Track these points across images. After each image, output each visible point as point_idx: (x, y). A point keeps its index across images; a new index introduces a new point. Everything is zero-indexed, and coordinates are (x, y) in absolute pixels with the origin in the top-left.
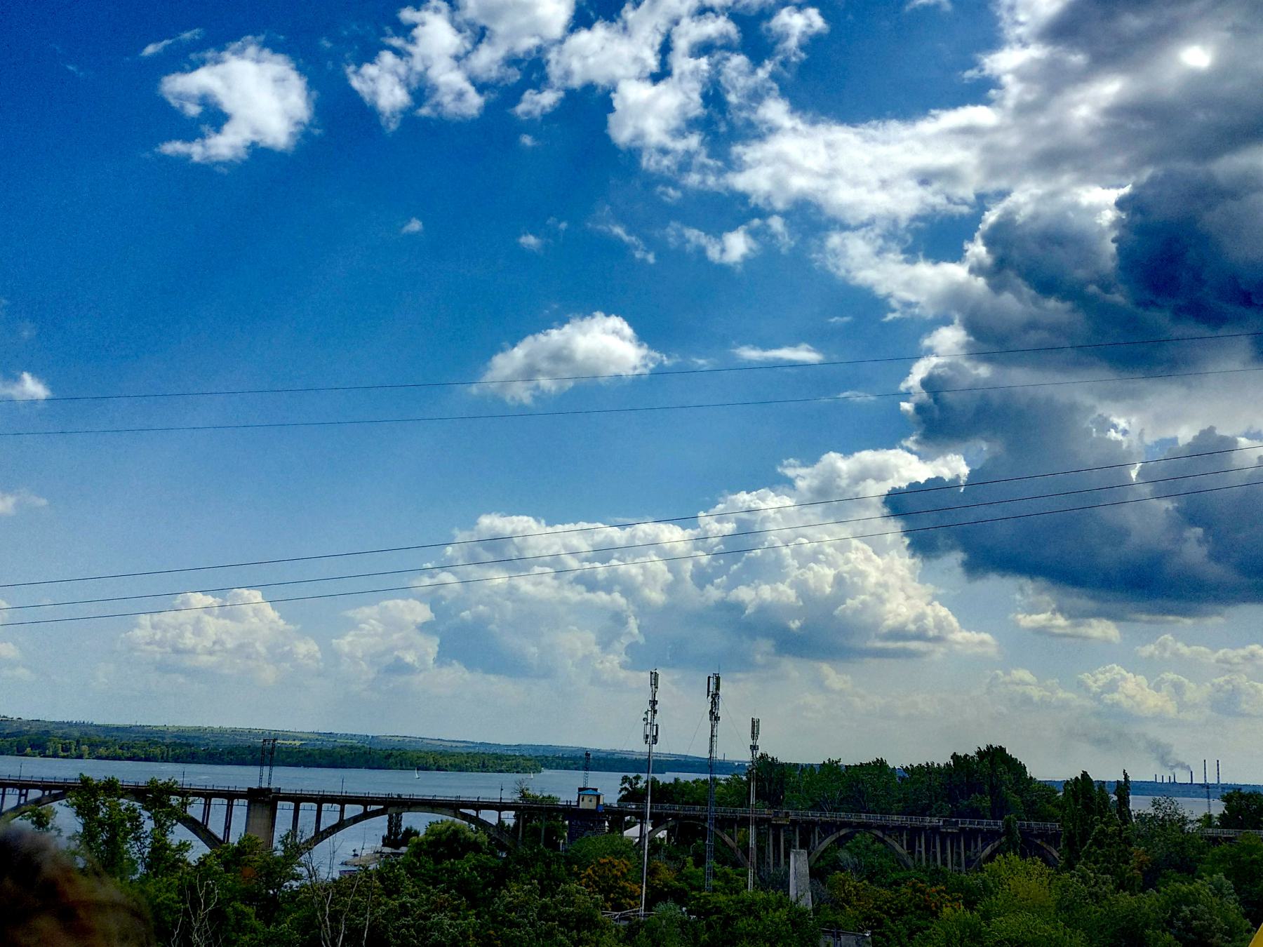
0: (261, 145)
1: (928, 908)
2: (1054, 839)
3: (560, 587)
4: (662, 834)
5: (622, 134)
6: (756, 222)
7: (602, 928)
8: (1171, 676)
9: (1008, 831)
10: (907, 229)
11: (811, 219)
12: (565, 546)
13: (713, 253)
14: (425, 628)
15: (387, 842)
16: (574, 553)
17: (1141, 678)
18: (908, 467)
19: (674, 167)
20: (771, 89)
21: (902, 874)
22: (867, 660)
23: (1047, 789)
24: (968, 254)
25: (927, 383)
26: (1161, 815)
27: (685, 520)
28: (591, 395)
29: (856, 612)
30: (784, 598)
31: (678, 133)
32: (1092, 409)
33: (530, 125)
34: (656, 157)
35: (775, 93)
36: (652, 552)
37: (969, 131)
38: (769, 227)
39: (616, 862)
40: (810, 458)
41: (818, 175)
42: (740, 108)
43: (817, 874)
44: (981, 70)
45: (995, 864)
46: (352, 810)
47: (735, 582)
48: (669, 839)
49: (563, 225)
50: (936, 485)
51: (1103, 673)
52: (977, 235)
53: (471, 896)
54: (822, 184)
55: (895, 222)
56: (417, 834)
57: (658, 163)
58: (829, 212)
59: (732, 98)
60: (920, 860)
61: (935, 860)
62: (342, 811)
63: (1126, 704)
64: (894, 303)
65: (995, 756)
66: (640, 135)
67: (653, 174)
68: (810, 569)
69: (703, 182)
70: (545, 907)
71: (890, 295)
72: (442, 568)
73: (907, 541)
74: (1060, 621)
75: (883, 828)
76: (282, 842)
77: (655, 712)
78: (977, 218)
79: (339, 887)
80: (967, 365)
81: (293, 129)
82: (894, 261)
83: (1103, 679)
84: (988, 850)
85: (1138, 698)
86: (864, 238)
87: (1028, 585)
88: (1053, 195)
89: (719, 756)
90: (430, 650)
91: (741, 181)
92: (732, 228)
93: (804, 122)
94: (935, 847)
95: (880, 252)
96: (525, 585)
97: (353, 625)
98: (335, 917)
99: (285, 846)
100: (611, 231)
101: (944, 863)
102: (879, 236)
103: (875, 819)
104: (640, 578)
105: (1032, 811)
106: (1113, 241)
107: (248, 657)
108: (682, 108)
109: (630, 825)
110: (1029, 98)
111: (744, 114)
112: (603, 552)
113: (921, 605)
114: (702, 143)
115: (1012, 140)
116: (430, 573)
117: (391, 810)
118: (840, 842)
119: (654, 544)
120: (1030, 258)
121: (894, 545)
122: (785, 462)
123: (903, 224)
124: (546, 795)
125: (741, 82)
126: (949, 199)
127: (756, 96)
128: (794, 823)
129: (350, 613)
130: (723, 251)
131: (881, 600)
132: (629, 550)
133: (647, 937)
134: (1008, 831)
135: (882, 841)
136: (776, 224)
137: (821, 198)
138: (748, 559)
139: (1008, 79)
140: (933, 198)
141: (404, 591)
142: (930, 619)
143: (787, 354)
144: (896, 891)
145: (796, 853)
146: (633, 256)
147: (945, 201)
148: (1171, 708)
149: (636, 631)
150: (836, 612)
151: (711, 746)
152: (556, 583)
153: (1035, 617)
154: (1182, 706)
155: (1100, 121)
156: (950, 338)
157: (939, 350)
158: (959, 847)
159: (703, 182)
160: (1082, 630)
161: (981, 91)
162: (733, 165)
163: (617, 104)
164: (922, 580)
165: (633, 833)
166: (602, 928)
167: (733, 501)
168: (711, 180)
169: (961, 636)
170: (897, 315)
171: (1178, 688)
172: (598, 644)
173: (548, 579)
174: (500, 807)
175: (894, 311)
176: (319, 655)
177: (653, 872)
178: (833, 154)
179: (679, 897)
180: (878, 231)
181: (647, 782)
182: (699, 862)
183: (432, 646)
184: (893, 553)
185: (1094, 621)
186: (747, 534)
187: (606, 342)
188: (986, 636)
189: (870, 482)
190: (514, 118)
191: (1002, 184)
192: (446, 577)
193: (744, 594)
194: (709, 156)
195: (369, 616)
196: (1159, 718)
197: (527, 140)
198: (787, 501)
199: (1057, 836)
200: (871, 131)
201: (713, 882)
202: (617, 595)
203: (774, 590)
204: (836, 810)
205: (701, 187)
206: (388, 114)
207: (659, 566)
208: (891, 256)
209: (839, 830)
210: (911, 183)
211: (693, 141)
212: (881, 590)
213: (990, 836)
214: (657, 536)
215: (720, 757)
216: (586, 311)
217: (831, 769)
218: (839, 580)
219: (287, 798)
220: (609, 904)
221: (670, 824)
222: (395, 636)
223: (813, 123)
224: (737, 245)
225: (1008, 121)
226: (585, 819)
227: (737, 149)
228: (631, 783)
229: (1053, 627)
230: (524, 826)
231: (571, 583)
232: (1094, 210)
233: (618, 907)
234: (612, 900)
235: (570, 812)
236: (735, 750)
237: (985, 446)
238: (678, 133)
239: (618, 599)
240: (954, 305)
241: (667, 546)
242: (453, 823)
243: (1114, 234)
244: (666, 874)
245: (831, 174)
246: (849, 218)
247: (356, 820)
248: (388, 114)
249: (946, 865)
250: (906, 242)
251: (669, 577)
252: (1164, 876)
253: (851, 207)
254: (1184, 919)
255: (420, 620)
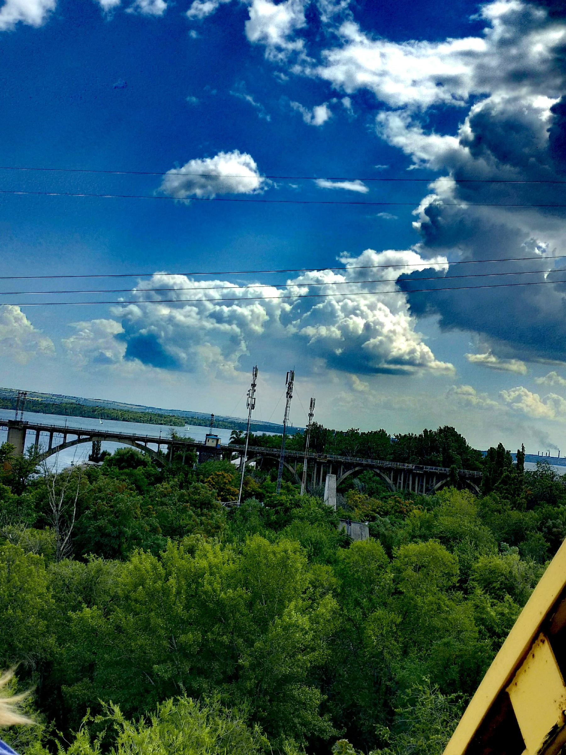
0: (25, 23)
1: (401, 512)
2: (477, 481)
3: (201, 319)
4: (253, 464)
5: (254, 36)
6: (335, 100)
7: (215, 508)
8: (554, 396)
9: (452, 475)
10: (426, 112)
11: (368, 101)
12: (206, 295)
13: (307, 118)
14: (120, 337)
15: (91, 458)
16: (211, 300)
17: (536, 396)
18: (412, 261)
19: (286, 60)
20: (348, 15)
21: (389, 494)
22: (379, 374)
23: (478, 453)
24: (460, 131)
25: (428, 211)
26: (541, 470)
27: (280, 285)
28: (227, 202)
29: (375, 346)
30: (334, 335)
31: (290, 38)
32: (527, 235)
33: (195, 24)
34: (274, 52)
35: (351, 18)
36: (257, 302)
37: (469, 54)
38: (342, 104)
39: (226, 475)
40: (356, 252)
41: (374, 74)
42: (328, 25)
43: (340, 490)
44: (480, 15)
45: (443, 492)
46: (71, 437)
47: (306, 323)
48: (257, 467)
49: (214, 92)
50: (429, 272)
51: (514, 391)
52: (467, 120)
53: (139, 488)
54: (376, 79)
55: (419, 107)
56: (109, 455)
57: (275, 56)
58: (380, 98)
59: (324, 19)
60: (400, 487)
61: (408, 487)
62: (65, 437)
63: (526, 410)
64: (415, 159)
65: (448, 433)
66: (265, 37)
67: (272, 63)
68: (351, 318)
69: (303, 71)
70: (182, 495)
71: (412, 154)
72: (130, 303)
73: (409, 306)
74: (493, 359)
75: (380, 468)
76: (28, 451)
77: (255, 391)
78: (468, 109)
79: (62, 477)
80: (455, 202)
81: (45, 15)
82: (416, 133)
83: (513, 395)
84: (439, 485)
85: (533, 407)
86: (400, 116)
87: (477, 337)
88: (515, 99)
89: (289, 424)
90: (121, 351)
91: (326, 73)
92: (319, 104)
93: (368, 38)
94: (409, 480)
95: (409, 127)
96: (179, 316)
97: (74, 331)
98: (58, 494)
99: (31, 454)
100: (245, 98)
101: (413, 489)
102: (408, 116)
103: (377, 462)
104: (250, 317)
105: (467, 465)
106: (548, 130)
107: (11, 345)
108: (292, 24)
109: (234, 458)
110: (508, 35)
111: (331, 30)
112: (229, 300)
113: (413, 344)
114: (305, 46)
115: (493, 62)
116: (123, 304)
117: (95, 439)
118: (355, 475)
119: (260, 298)
120: (497, 136)
121: (401, 307)
122: (341, 254)
123: (424, 110)
124: (187, 437)
125: (330, 8)
126: (454, 97)
127: (338, 19)
128: (329, 462)
129: (73, 324)
130: (313, 117)
131: (391, 340)
132: (245, 301)
133: (240, 515)
134: (452, 475)
135: (378, 475)
136: (347, 102)
137: (376, 89)
138: (315, 309)
139: (496, 22)
140: (444, 94)
141: (108, 316)
142: (418, 353)
143: (347, 185)
144: (385, 502)
145: (330, 476)
146: (258, 116)
147: (450, 97)
148: (551, 414)
149: (245, 349)
150: (363, 346)
151: (286, 412)
152: (198, 317)
153: (478, 356)
154: (558, 413)
155: (549, 56)
156: (445, 185)
157: (438, 191)
158: (423, 482)
159: (303, 71)
160: (506, 366)
161: (478, 29)
162: (323, 62)
163: (252, 14)
164: (416, 330)
165: (237, 462)
166: (215, 508)
167: (307, 275)
168: (308, 71)
169: (434, 364)
170: (416, 167)
171: (556, 403)
172: (222, 354)
173: (194, 314)
174: (160, 442)
175: (414, 164)
176: (54, 349)
177: (246, 483)
178: (384, 61)
179: (260, 496)
180: (409, 113)
181: (246, 434)
182: (274, 479)
183: (122, 348)
184: (401, 314)
185: (513, 361)
186: (315, 294)
187: (237, 170)
188: (450, 365)
189: (391, 269)
190: (185, 19)
191: (486, 89)
192: (134, 308)
193: (310, 331)
194: (308, 55)
195: (85, 327)
196: (544, 419)
197: (193, 34)
198: (340, 279)
199: (480, 478)
200: (409, 48)
201: (280, 491)
202: (235, 327)
203: (328, 330)
204: (354, 456)
205: (301, 74)
206: (106, 9)
207: (259, 309)
208: (415, 129)
209: (355, 467)
210: (431, 84)
211: (299, 44)
212: (391, 334)
213: (440, 477)
214: (261, 293)
215: (289, 425)
216: (228, 150)
217: (353, 434)
218: (367, 326)
219: (32, 427)
220: (219, 498)
221: (259, 458)
222: (101, 341)
223: (374, 39)
224: (322, 114)
225: (494, 50)
226: (209, 451)
227: (325, 52)
228: (237, 435)
229: (488, 362)
230: (173, 455)
231: (207, 317)
232: (538, 111)
233: (224, 500)
234: (222, 496)
235: (201, 447)
236: (299, 421)
237: (460, 253)
238: (290, 38)
239: (236, 328)
240: (449, 164)
241: (267, 300)
242: (131, 449)
243: (549, 126)
244: (254, 484)
245: (383, 74)
246: (391, 102)
247: (73, 443)
248: (106, 9)
249: (414, 491)
250: (425, 121)
251: (267, 318)
252: (539, 504)
253: (392, 96)
254: (548, 528)
255: (116, 332)
